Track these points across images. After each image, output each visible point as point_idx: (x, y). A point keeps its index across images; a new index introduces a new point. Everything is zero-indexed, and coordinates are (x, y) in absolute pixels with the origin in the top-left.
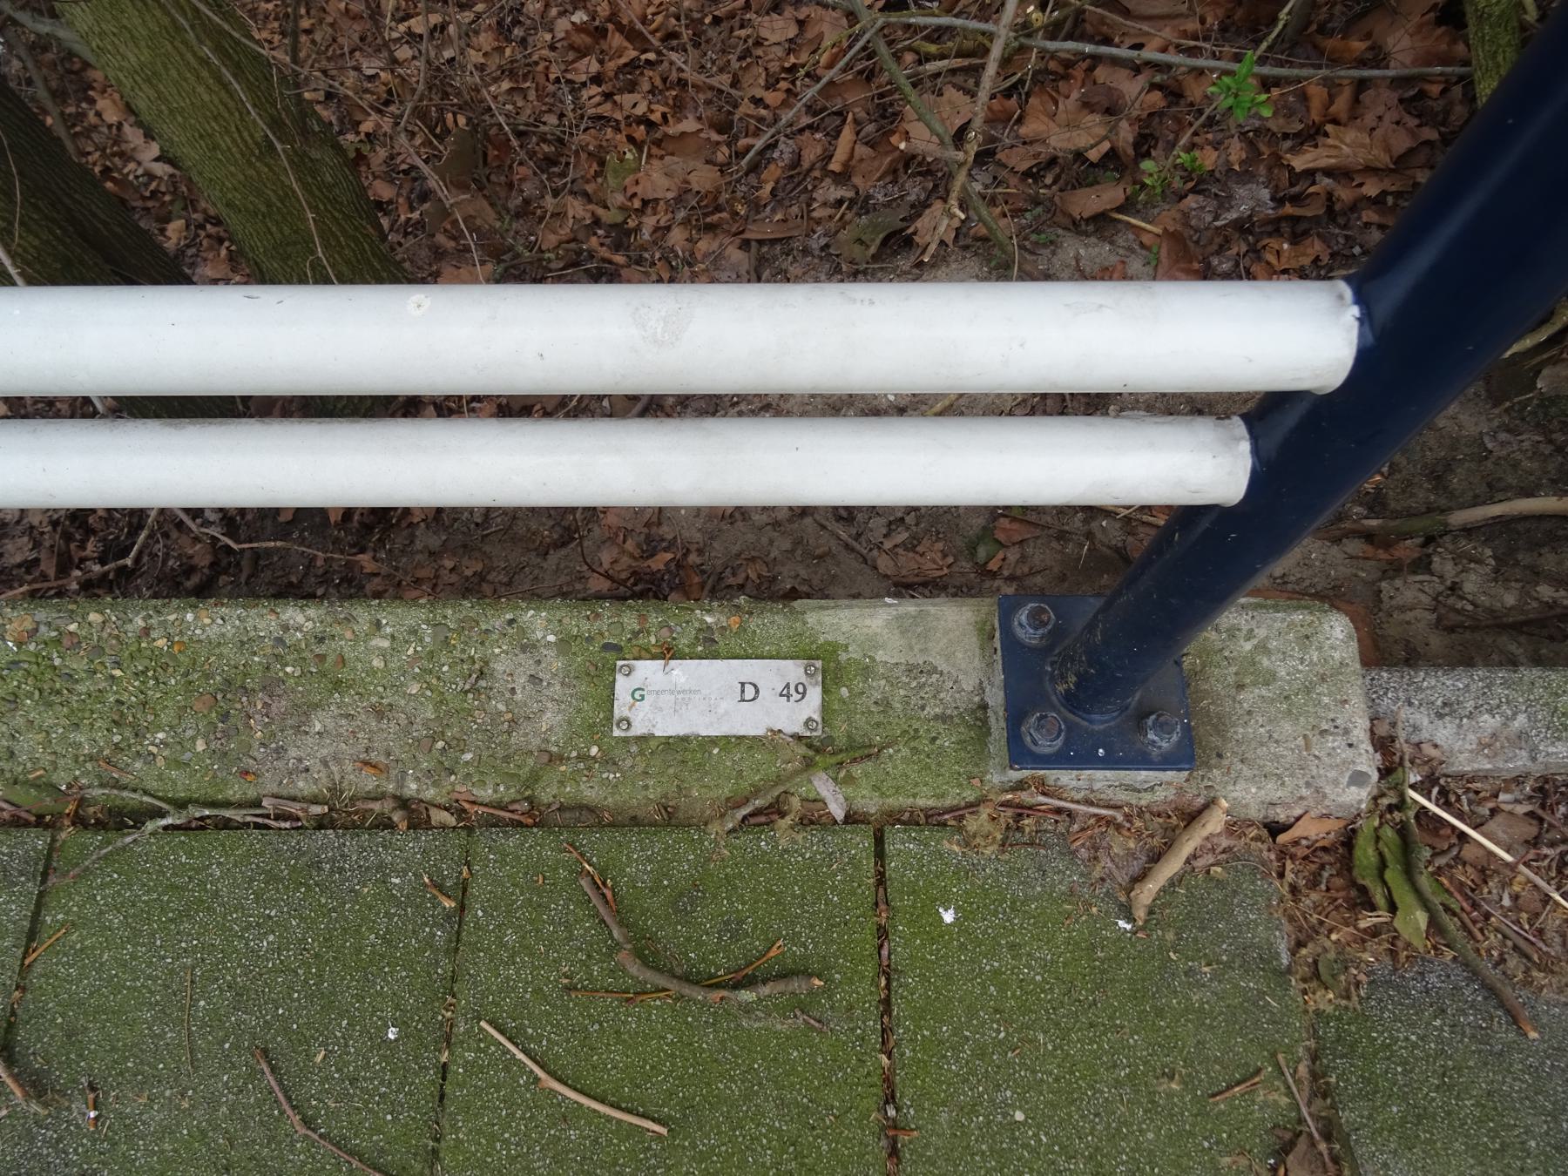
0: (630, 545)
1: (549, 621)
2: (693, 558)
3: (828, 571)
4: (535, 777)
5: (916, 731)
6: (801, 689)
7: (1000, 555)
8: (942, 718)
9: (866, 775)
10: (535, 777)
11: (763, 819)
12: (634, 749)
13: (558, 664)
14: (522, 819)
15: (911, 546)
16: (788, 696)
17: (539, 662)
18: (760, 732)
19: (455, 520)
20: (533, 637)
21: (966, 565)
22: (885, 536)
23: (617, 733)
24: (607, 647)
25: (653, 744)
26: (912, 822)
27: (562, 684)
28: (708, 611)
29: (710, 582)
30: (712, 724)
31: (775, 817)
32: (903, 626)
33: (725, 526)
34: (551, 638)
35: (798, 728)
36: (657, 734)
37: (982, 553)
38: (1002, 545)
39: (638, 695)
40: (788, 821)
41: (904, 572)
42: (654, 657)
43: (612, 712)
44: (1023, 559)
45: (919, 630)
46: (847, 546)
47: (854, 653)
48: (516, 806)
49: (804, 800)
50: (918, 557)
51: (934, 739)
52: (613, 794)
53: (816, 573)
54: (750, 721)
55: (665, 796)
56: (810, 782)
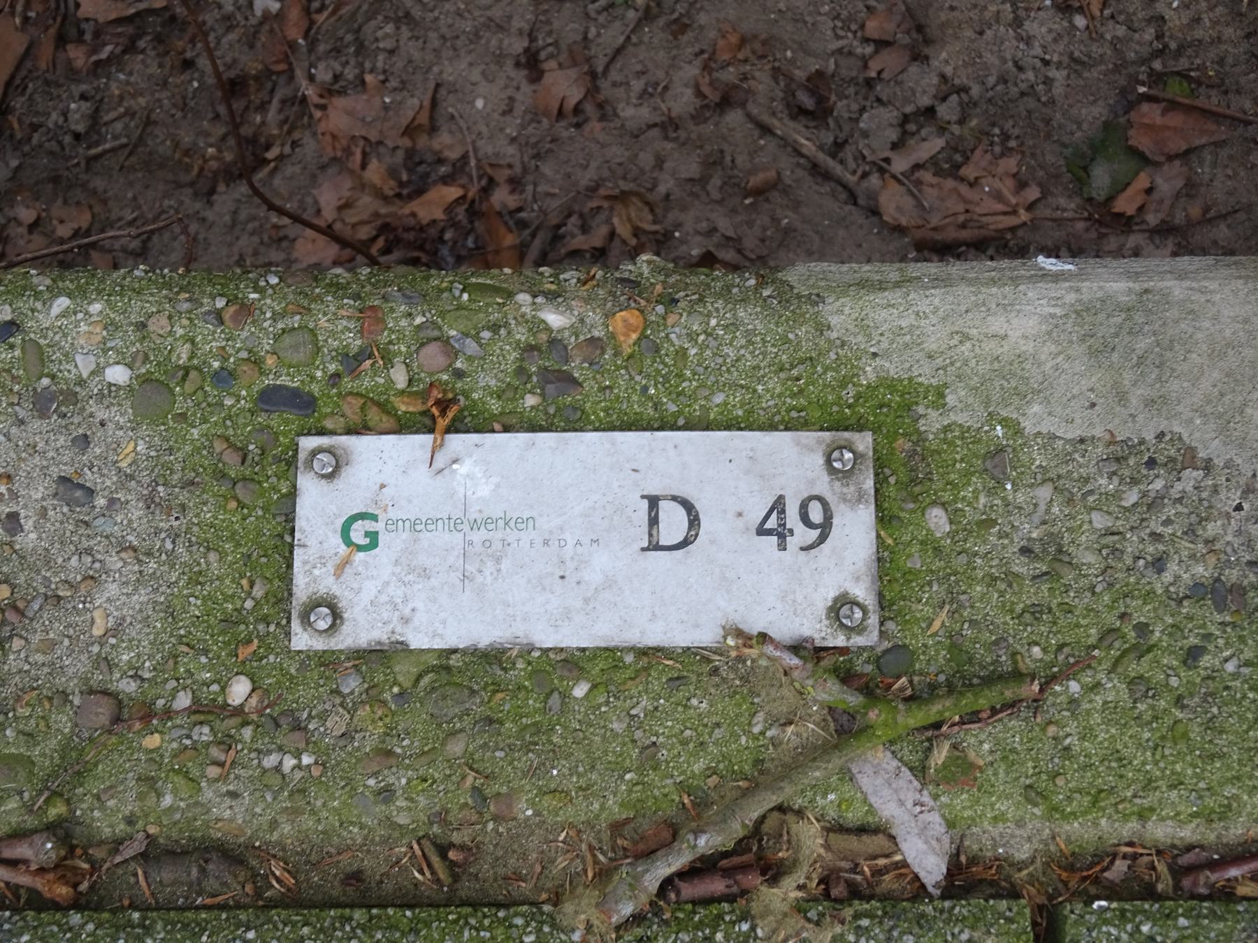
0: (375, 172)
1: (111, 326)
2: (502, 197)
3: (775, 220)
4: (73, 768)
5: (1143, 629)
6: (816, 514)
7: (1143, 181)
8: (1216, 593)
9: (1007, 756)
10: (73, 768)
11: (718, 886)
12: (351, 684)
13: (136, 448)
14: (39, 884)
15: (949, 166)
16: (782, 534)
17: (84, 442)
18: (705, 635)
19: (35, 127)
20: (69, 372)
21: (1068, 205)
22: (895, 146)
23: (302, 640)
24: (271, 398)
25: (404, 671)
26: (1138, 890)
27: (150, 502)
28: (552, 296)
29: (537, 245)
30: (567, 614)
31: (752, 879)
32: (1093, 334)
33: (564, 131)
34: (118, 374)
35: (811, 625)
36: (418, 641)
37: (1101, 177)
38: (1143, 160)
39: (361, 534)
40: (787, 891)
41: (935, 221)
42: (403, 427)
43: (286, 576)
44: (1190, 188)
45: (1142, 344)
46: (815, 169)
47: (962, 410)
48: (22, 850)
49: (837, 828)
50: (964, 189)
51: (1193, 655)
52: (295, 812)
53: (750, 224)
54: (674, 607)
55: (442, 817)
56: (847, 776)
